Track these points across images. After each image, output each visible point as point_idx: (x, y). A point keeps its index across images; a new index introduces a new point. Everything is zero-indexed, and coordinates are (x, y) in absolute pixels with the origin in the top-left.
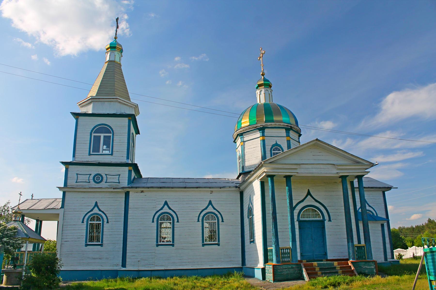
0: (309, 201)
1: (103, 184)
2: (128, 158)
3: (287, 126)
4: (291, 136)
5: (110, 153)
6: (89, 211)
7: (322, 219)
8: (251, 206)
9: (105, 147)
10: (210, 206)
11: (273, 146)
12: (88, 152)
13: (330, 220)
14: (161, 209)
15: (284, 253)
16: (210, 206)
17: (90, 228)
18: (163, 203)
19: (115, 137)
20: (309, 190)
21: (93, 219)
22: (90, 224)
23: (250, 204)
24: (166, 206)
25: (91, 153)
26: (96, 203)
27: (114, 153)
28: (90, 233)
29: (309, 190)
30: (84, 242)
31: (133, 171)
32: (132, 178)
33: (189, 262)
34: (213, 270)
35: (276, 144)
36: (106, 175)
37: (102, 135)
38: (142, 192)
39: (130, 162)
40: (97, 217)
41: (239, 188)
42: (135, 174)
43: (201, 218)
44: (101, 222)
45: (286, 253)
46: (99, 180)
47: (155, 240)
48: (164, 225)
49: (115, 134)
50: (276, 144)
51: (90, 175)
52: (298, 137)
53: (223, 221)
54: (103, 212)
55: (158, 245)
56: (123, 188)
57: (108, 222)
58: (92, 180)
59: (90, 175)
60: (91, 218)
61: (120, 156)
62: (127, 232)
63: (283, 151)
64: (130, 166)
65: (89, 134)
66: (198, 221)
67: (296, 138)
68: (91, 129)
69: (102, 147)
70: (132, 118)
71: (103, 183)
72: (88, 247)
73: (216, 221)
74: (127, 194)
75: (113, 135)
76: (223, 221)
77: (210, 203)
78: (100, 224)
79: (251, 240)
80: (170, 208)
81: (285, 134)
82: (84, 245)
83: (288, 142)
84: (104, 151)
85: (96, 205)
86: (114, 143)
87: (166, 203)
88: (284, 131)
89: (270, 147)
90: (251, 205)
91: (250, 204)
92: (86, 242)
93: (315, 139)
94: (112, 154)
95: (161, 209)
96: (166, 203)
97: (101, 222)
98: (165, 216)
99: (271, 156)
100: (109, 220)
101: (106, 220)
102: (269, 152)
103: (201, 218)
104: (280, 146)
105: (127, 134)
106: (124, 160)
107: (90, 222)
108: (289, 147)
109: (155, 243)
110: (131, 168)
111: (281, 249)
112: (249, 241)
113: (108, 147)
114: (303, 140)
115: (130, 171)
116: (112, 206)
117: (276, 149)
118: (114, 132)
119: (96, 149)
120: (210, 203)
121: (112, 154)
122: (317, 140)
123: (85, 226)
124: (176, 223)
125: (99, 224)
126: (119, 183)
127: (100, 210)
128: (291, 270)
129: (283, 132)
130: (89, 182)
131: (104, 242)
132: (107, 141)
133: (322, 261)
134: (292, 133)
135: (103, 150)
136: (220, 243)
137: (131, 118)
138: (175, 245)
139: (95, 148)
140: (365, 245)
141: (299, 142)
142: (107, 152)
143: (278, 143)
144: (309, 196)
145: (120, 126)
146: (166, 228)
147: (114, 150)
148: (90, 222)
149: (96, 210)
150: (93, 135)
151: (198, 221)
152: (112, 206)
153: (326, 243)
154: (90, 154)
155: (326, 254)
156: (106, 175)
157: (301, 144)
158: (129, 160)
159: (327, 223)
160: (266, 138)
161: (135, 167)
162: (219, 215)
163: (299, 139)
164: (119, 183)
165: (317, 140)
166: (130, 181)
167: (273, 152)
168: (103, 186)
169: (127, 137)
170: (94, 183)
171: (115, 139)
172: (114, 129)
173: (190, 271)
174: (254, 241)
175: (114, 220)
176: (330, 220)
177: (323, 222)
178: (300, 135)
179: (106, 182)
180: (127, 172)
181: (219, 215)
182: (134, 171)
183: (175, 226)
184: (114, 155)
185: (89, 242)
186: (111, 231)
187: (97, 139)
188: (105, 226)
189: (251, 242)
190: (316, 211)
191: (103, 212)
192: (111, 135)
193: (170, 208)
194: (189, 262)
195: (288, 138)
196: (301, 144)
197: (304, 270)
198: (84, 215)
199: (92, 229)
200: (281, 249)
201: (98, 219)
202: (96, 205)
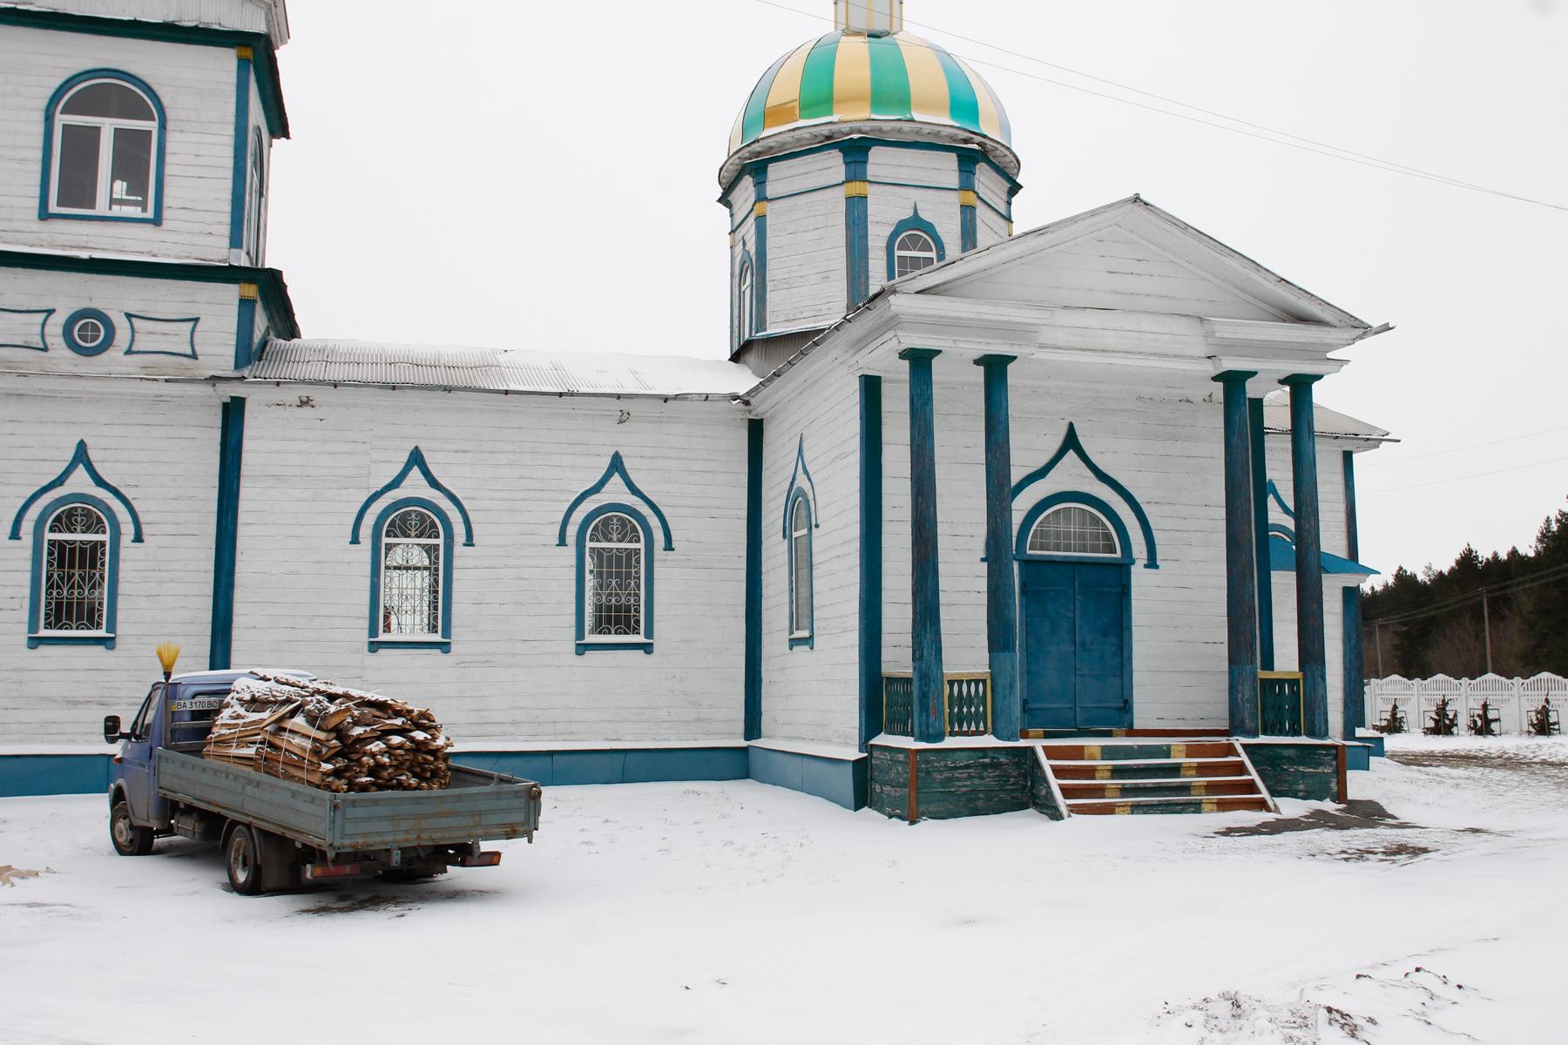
0: (1070, 476)
1: (115, 358)
2: (236, 241)
3: (966, 141)
4: (979, 188)
5: (150, 214)
6: (45, 483)
7: (1118, 555)
8: (806, 486)
9: (120, 187)
10: (616, 478)
11: (902, 226)
12: (36, 203)
13: (1152, 563)
14: (395, 484)
15: (960, 700)
16: (616, 478)
17: (50, 564)
18: (405, 457)
19: (171, 137)
20: (1071, 426)
21: (604, 532)
22: (52, 543)
23: (800, 475)
24: (416, 472)
25: (53, 208)
26: (82, 448)
27: (166, 214)
28: (50, 587)
29: (1071, 426)
30: (25, 628)
31: (259, 307)
32: (258, 336)
33: (513, 723)
34: (621, 757)
35: (916, 224)
36: (129, 316)
37: (108, 127)
38: (305, 403)
39: (244, 262)
40: (88, 514)
41: (747, 403)
42: (270, 319)
43: (572, 531)
44: (106, 538)
45: (969, 701)
46: (94, 338)
47: (366, 623)
48: (397, 557)
49: (170, 125)
50: (916, 224)
51: (50, 312)
52: (1005, 197)
53: (669, 547)
54: (116, 492)
55: (375, 646)
56: (214, 380)
57: (138, 538)
58: (61, 340)
59: (50, 312)
60: (58, 519)
61: (194, 232)
62: (231, 585)
63: (941, 257)
64: (250, 281)
65: (40, 116)
66: (562, 542)
67: (995, 198)
68: (50, 92)
69: (108, 186)
70: (257, 55)
71: (115, 354)
72: (44, 650)
73: (641, 546)
74: (233, 413)
75: (163, 127)
76: (469, 542)
77: (617, 465)
78: (103, 544)
79: (797, 634)
80: (434, 484)
81: (953, 179)
82: (25, 641)
83: (968, 211)
84: (116, 208)
85: (81, 455)
86: (168, 170)
87: (416, 458)
88: (951, 160)
89: (889, 230)
90: (802, 481)
91: (800, 475)
92: (33, 626)
93: (1131, 194)
94: (157, 221)
95: (395, 484)
96: (416, 458)
97: (106, 538)
98: (414, 521)
99: (891, 276)
100: (146, 529)
101: (128, 529)
102: (883, 254)
103: (572, 531)
104: (928, 228)
105: (231, 130)
106: (217, 251)
107: (49, 536)
108: (969, 238)
109: (364, 637)
110: (251, 291)
111: (951, 683)
112: (786, 636)
113: (137, 186)
114: (1028, 211)
115: (246, 305)
116: (161, 473)
117: (913, 243)
118: (170, 114)
119: (75, 186)
120: (617, 465)
121: (157, 221)
122: (1136, 199)
123: (29, 553)
124: (459, 549)
125: (97, 546)
126: (194, 356)
127: (100, 482)
128: (991, 773)
129: (946, 168)
130: (45, 349)
131: (121, 629)
132: (135, 160)
133: (1109, 734)
134: (985, 178)
135: (112, 201)
136: (657, 641)
137: (248, 53)
138: (454, 647)
139: (75, 186)
140: (1300, 676)
141: (1008, 219)
142: (135, 212)
143: (923, 215)
144: (1071, 455)
145: (198, 87)
146: (407, 568)
147: (167, 201)
148: (49, 536)
149: (80, 482)
150: (61, 119)
151: (562, 542)
152: (161, 473)
153: (1130, 659)
154: (44, 215)
155: (1126, 707)
156: (129, 316)
157: (1017, 230)
158: (243, 254)
159: (1140, 576)
160: (871, 190)
161: (271, 288)
162: (654, 521)
163: (1009, 203)
164: (194, 356)
165: (1136, 199)
166: (249, 353)
167: (898, 253)
168: (117, 370)
169: (230, 141)
170: (69, 353)
171: (170, 147)
172: (166, 101)
173: (517, 761)
174: (811, 637)
175: (170, 529)
176: (1152, 563)
177: (1122, 570)
178: (1015, 188)
179: (129, 352)
180: (234, 309)
181: (654, 521)
182: (267, 307)
183: (456, 563)
184: (166, 224)
185: (48, 626)
186: (158, 591)
187: (81, 146)
188: (123, 554)
189: (794, 642)
190: (1096, 521)
191: (116, 492)
192: (152, 126)
193: (434, 484)
194: (513, 723)
195: (970, 198)
196: (1017, 230)
197: (950, 742)
198: (22, 502)
199: (61, 565)
200: (951, 683)
201: (627, 533)
202: (81, 455)
